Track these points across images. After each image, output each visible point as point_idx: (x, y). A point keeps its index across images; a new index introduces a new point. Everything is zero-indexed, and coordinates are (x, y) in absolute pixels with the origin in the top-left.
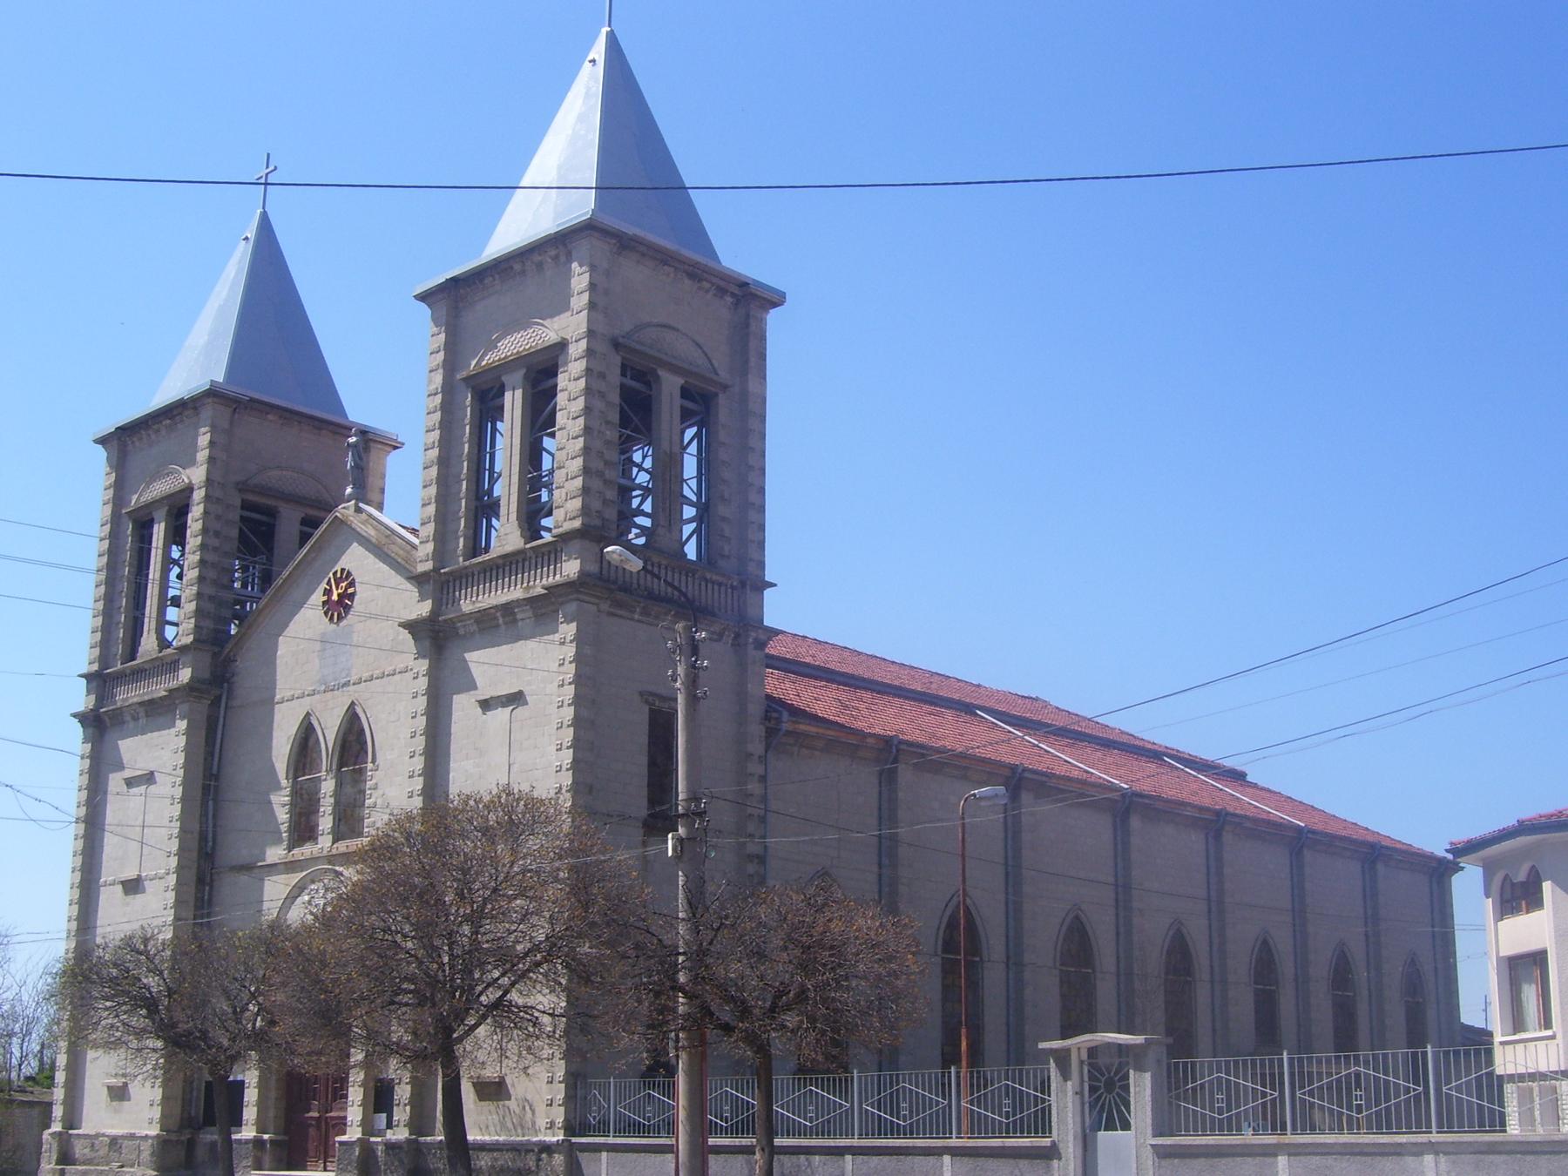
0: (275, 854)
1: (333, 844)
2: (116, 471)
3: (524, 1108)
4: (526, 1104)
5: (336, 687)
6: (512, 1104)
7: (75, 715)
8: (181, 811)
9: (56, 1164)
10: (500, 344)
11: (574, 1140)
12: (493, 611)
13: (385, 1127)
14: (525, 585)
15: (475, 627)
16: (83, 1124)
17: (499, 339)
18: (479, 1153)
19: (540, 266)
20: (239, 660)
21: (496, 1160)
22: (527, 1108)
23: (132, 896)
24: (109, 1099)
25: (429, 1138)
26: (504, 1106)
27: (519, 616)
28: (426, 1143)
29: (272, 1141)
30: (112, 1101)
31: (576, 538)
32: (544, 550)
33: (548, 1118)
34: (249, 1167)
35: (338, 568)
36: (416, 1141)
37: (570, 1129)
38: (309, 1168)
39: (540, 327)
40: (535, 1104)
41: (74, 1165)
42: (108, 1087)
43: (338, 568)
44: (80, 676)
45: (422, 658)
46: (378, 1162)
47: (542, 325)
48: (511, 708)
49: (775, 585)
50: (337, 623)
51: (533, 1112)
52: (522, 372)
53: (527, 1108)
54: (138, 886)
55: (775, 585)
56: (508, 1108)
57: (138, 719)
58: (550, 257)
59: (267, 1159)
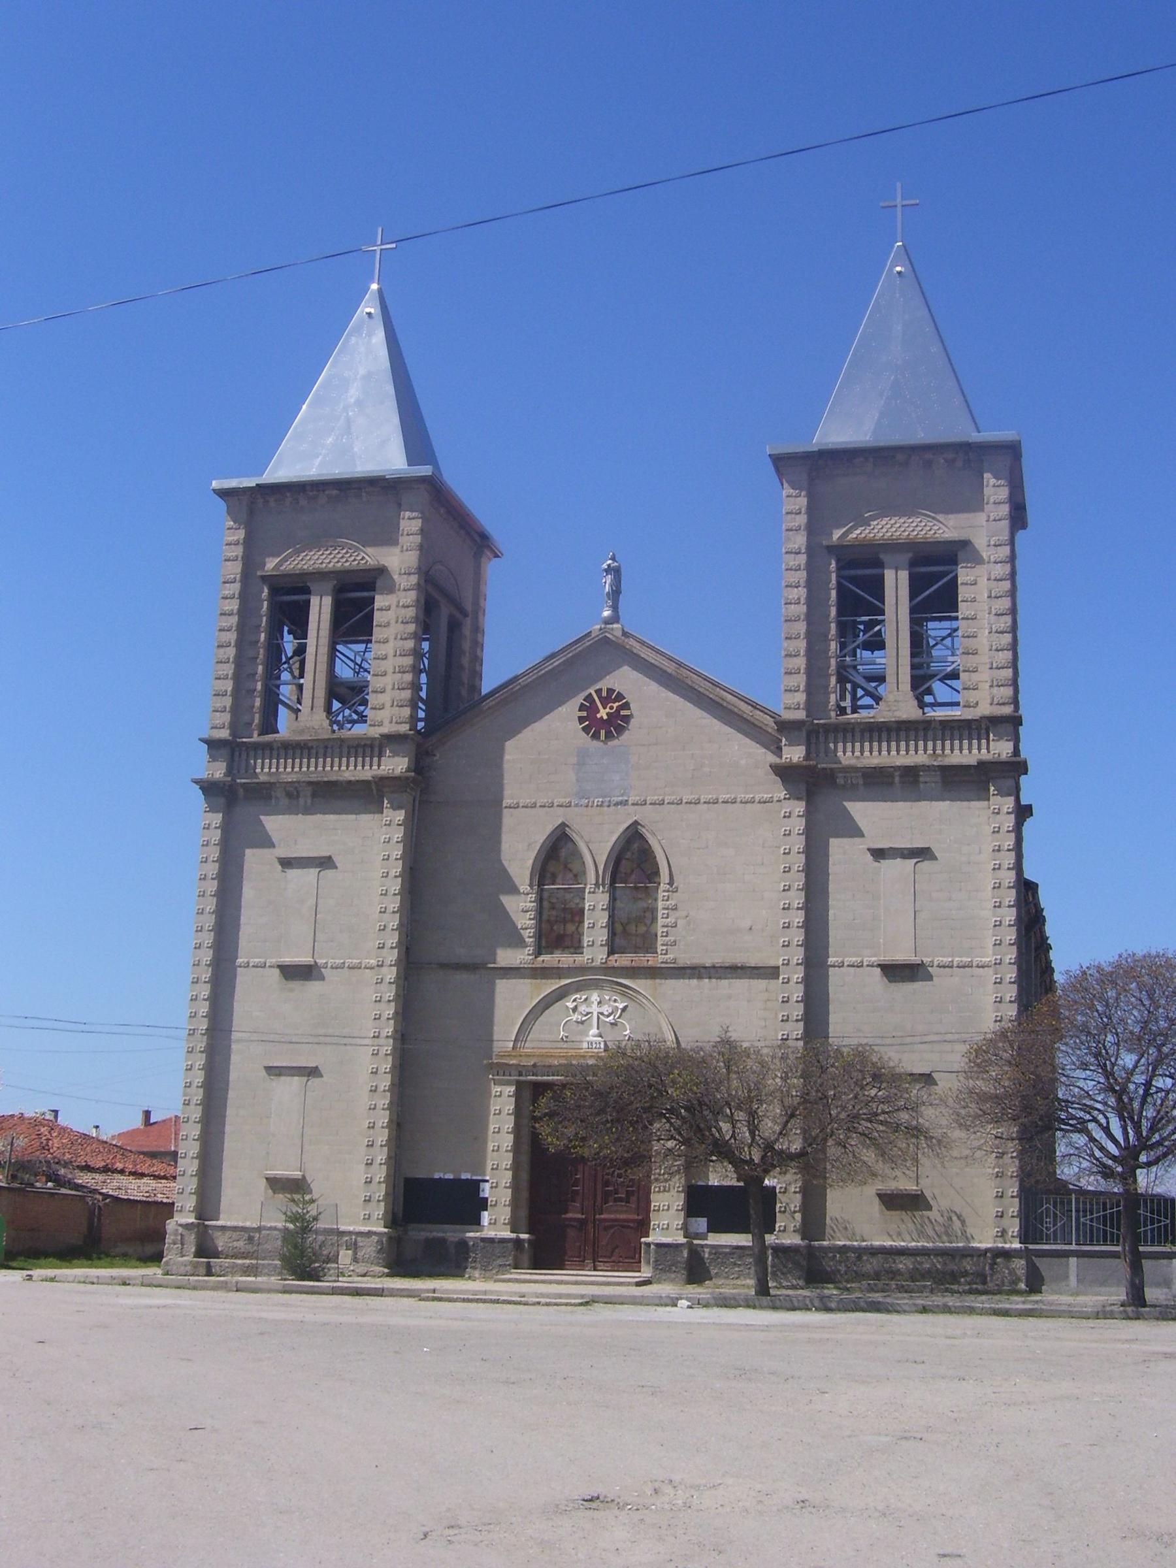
0: (520, 957)
1: (608, 956)
2: (245, 528)
3: (950, 1219)
4: (953, 1215)
5: (607, 804)
6: (934, 1214)
7: (196, 782)
8: (401, 903)
9: (194, 1257)
10: (875, 523)
11: (1031, 1247)
12: (892, 769)
13: (706, 1231)
14: (930, 752)
15: (861, 782)
16: (221, 1216)
17: (873, 518)
18: (896, 1257)
19: (928, 464)
20: (438, 755)
21: (921, 1263)
22: (955, 1218)
23: (302, 982)
24: (270, 1191)
25: (816, 1243)
26: (922, 1217)
27: (922, 779)
28: (822, 1248)
29: (529, 1241)
30: (274, 1193)
31: (1008, 722)
32: (954, 725)
33: (998, 1227)
34: (509, 1265)
35: (604, 684)
36: (809, 1247)
37: (1025, 1237)
38: (567, 1267)
39: (941, 525)
40: (964, 1215)
41: (218, 1258)
42: (267, 1179)
43: (604, 684)
44: (201, 740)
45: (794, 799)
46: (705, 1264)
47: (934, 518)
48: (915, 860)
49: (200, 740)
50: (605, 742)
51: (963, 1222)
52: (910, 555)
53: (955, 1218)
54: (315, 973)
55: (200, 740)
56: (928, 1218)
57: (298, 796)
58: (946, 460)
59: (525, 1258)
